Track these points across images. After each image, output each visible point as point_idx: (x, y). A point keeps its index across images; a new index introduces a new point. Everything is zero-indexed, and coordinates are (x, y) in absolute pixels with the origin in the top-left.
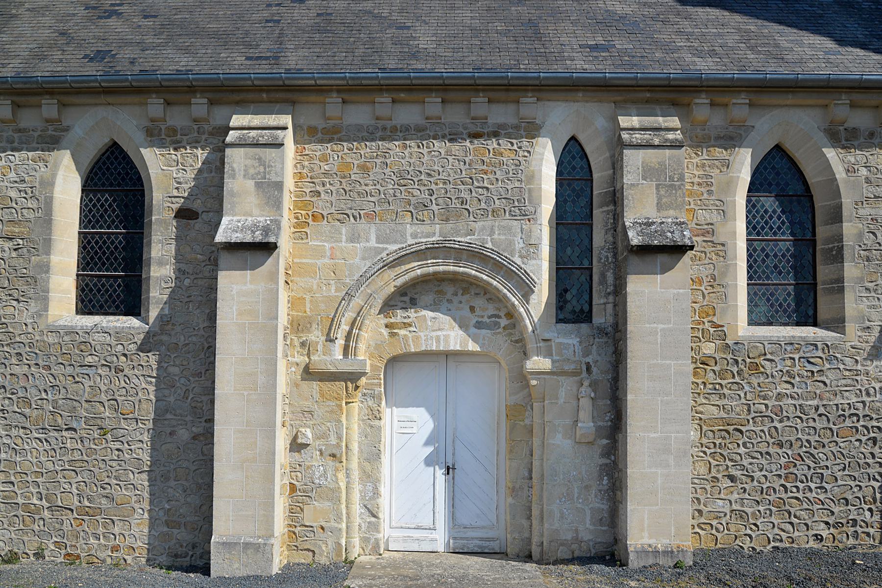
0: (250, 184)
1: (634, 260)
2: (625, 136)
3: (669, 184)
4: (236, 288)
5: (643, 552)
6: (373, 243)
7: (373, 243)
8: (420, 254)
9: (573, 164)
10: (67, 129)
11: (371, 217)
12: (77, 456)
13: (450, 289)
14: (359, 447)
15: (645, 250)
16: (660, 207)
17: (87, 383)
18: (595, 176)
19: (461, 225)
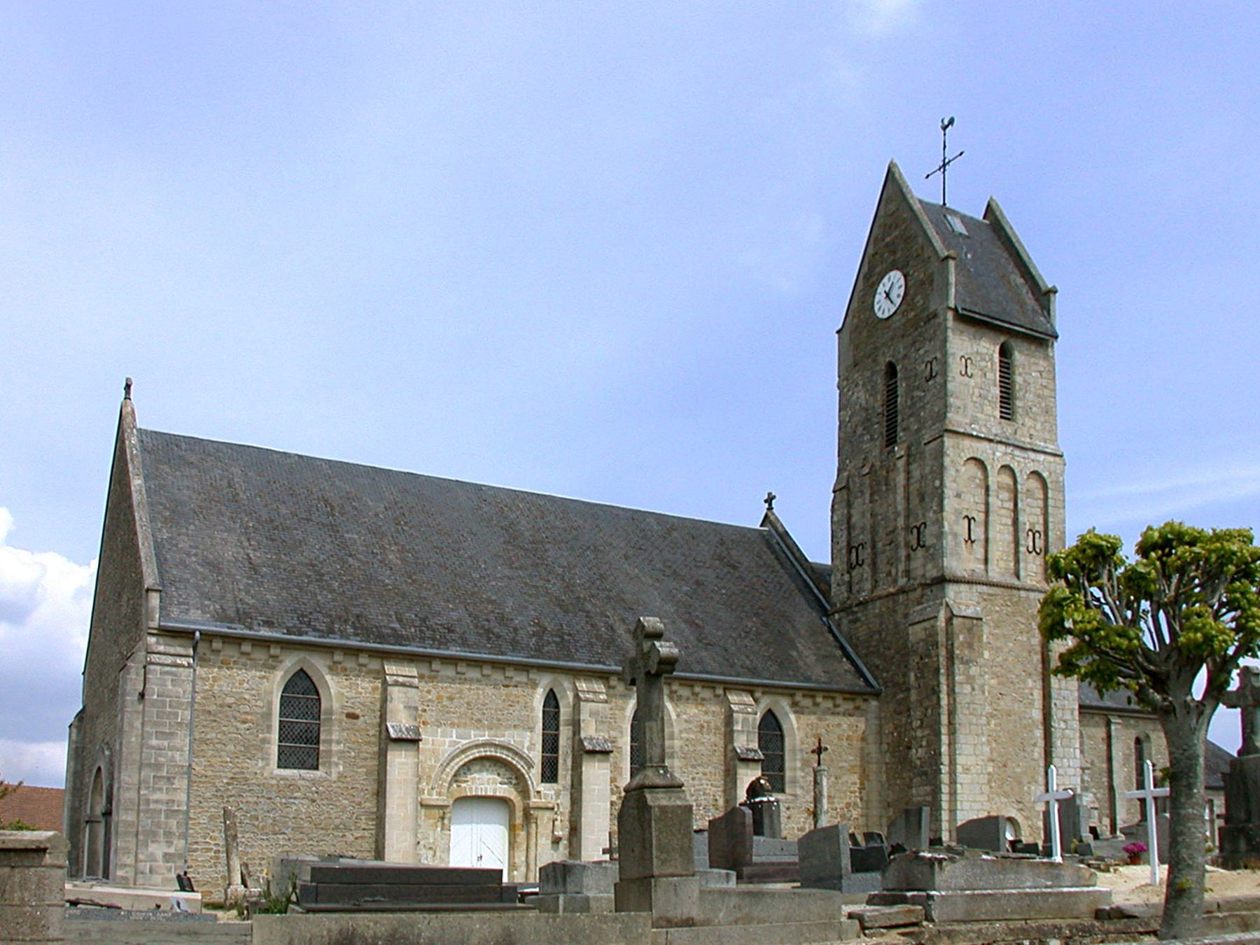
0: (401, 706)
1: (585, 757)
2: (581, 695)
3: (601, 720)
4: (397, 760)
5: (995, 344)
6: (454, 738)
7: (454, 738)
8: (484, 745)
9: (552, 700)
10: (281, 662)
11: (453, 725)
12: (286, 848)
13: (487, 764)
14: (939, 699)
15: (592, 753)
16: (597, 730)
17: (294, 808)
18: (562, 710)
19: (499, 733)
